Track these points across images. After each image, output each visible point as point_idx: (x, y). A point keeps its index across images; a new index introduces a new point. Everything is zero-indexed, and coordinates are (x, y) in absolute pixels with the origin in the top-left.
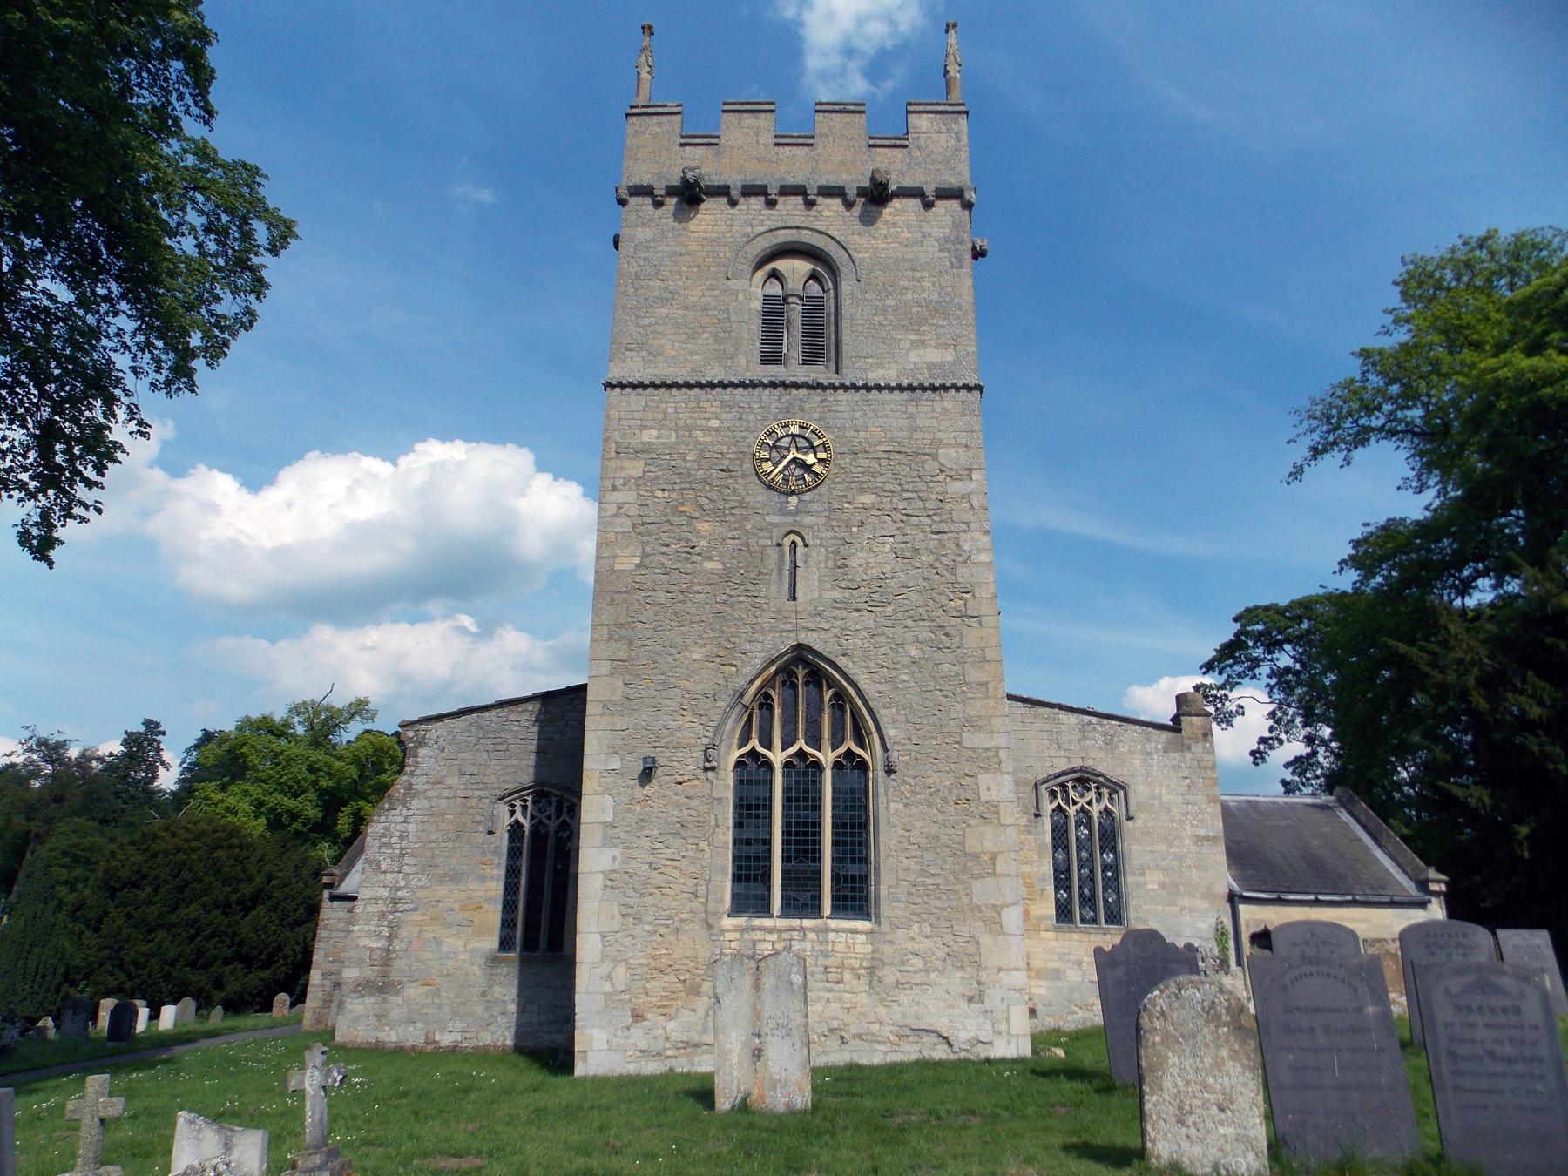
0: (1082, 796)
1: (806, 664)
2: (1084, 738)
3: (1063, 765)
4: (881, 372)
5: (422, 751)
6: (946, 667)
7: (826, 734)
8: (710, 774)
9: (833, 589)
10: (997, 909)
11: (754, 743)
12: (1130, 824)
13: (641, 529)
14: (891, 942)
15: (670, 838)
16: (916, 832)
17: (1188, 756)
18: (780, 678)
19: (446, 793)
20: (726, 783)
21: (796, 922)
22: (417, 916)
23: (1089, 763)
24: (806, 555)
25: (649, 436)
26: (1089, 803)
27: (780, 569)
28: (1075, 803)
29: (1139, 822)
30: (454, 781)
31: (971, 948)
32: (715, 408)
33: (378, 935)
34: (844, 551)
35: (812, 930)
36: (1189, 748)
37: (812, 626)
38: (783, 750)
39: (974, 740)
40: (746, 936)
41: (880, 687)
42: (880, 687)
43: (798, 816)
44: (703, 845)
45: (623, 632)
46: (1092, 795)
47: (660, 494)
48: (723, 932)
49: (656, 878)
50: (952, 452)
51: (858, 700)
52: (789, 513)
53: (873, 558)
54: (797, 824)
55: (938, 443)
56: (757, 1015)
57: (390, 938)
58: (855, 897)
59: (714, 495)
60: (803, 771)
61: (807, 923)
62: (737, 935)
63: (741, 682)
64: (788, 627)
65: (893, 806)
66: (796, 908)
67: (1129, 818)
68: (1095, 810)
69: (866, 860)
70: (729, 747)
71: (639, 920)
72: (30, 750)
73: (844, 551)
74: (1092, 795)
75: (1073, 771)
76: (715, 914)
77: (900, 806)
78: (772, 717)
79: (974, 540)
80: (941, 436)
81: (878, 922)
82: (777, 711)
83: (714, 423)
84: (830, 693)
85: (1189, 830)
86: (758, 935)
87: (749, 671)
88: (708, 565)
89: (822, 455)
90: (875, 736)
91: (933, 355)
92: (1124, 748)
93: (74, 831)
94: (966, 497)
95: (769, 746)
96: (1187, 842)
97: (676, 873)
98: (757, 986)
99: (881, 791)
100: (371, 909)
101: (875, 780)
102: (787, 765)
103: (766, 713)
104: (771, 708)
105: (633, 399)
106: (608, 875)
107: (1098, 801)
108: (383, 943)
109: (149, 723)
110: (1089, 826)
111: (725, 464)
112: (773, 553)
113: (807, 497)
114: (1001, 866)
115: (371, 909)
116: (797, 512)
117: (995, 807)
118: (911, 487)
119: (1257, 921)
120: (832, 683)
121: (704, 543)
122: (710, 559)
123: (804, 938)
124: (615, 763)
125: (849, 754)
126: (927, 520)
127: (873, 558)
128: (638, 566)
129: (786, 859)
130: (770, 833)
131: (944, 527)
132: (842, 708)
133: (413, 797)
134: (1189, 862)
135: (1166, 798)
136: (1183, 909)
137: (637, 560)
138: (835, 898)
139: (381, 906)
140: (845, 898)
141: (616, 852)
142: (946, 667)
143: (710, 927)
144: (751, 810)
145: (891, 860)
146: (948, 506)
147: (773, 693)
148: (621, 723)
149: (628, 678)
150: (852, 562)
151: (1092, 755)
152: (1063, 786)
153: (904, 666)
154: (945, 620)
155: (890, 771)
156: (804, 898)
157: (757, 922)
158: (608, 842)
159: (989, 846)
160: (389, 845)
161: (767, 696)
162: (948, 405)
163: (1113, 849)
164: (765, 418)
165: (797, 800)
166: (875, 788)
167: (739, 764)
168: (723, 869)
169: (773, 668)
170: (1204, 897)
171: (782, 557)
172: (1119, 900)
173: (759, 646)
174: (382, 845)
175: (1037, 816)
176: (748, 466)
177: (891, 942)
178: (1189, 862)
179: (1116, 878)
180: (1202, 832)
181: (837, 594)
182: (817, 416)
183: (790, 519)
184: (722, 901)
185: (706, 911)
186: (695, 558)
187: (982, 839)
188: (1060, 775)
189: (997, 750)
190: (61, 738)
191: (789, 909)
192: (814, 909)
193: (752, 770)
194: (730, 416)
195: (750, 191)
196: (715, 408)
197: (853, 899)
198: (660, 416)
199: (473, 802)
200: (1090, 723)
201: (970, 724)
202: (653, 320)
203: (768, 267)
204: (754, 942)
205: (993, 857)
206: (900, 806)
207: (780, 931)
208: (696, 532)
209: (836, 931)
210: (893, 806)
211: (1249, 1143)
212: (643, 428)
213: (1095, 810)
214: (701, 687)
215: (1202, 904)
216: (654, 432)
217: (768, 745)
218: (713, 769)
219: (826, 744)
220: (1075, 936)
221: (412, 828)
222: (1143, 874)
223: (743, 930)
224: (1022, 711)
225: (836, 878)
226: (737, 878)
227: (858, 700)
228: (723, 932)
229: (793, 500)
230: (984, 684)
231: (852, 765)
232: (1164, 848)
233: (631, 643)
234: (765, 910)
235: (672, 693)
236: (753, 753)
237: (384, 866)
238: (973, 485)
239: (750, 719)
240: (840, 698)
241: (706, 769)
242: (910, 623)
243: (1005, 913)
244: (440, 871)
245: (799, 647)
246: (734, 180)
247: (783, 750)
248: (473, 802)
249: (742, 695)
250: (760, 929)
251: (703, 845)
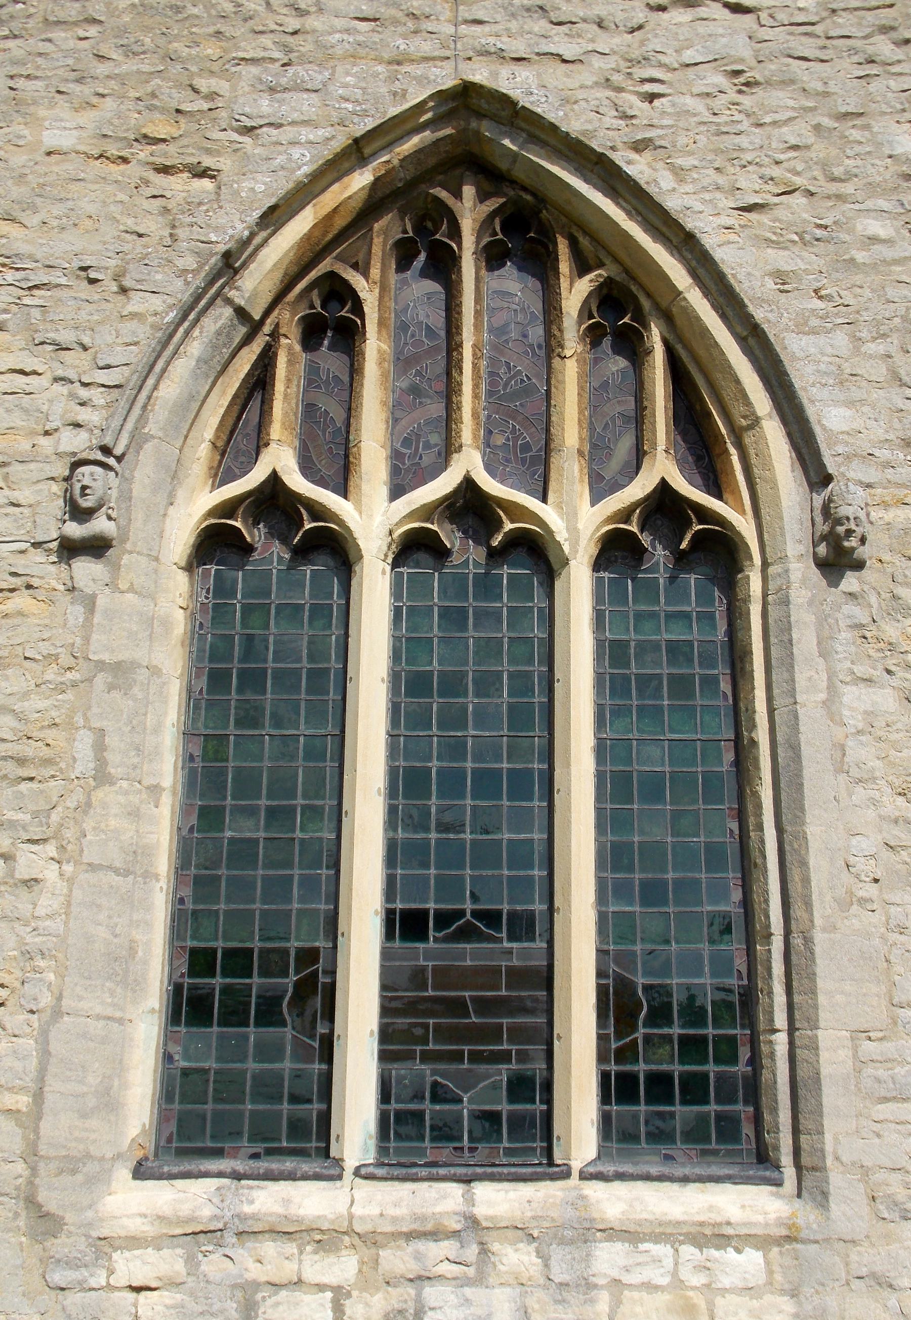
1: (491, 175)
7: (570, 432)
8: (85, 569)
11: (281, 459)
14: (882, 1283)
18: (386, 230)
20: (155, 603)
21: (442, 1199)
35: (521, 1231)
37: (518, 47)
38: (397, 492)
40: (213, 1265)
41: (781, 259)
42: (781, 259)
43: (456, 750)
48: (104, 1246)
51: (697, 301)
54: (452, 783)
58: (703, 1078)
61: (496, 1199)
62: (166, 1262)
63: (231, 225)
64: (427, 47)
65: (854, 698)
66: (445, 1132)
70: (174, 474)
76: (71, 1165)
77: (885, 699)
78: (355, 370)
81: (810, 1177)
84: (584, 286)
86: (271, 1260)
87: (263, 188)
90: (773, 436)
99: (805, 639)
101: (777, 600)
103: (330, 361)
104: (348, 336)
120: (595, 247)
123: (482, 1271)
125: (664, 506)
130: (332, 925)
132: (631, 345)
138: (616, 1088)
140: (660, 1087)
143: (44, 1222)
145: (859, 919)
147: (358, 282)
153: (872, 189)
155: (837, 558)
156: (485, 1089)
157: (268, 1199)
161: (338, 292)
165: (452, 684)
166: (779, 632)
167: (217, 544)
168: (121, 965)
169: (361, 180)
173: (305, 105)
177: (882, 1283)
184: (109, 1103)
185: (32, 1154)
191: (415, 1135)
192: (521, 1135)
193: (268, 544)
197: (694, 1090)
206: (885, 699)
207: (372, 1240)
209: (629, 1235)
210: (854, 698)
214: (68, 246)
218: (97, 547)
219: (570, 469)
223: (202, 1236)
226: (188, 1007)
227: (697, 301)
228: (104, 1246)
231: (681, 548)
236: (273, 501)
239: (260, 382)
241: (70, 549)
243: (480, 1211)
245: (465, 100)
247: (397, 492)
249: (230, 264)
250: (284, 1231)
251: (30, 861)
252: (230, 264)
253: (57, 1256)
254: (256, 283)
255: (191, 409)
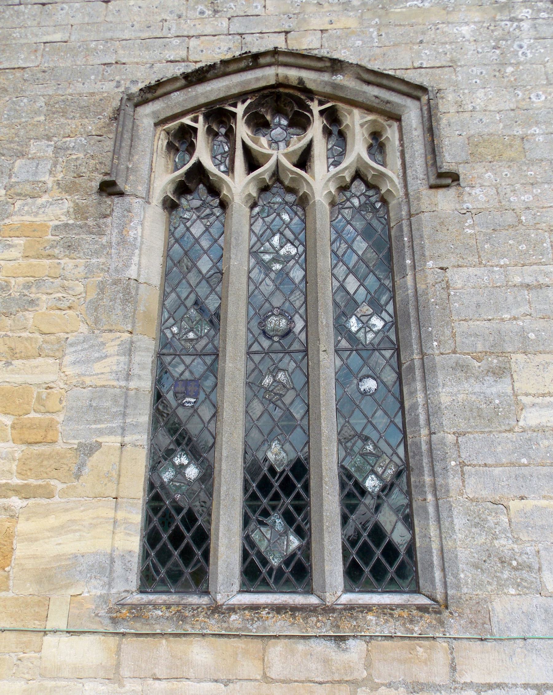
12: (445, 201)
26: (304, 160)
29: (479, 191)
61: (194, 599)
67: (445, 179)
107: (335, 159)
175: (108, 188)
211: (259, 675)
220: (200, 653)
222: (501, 372)
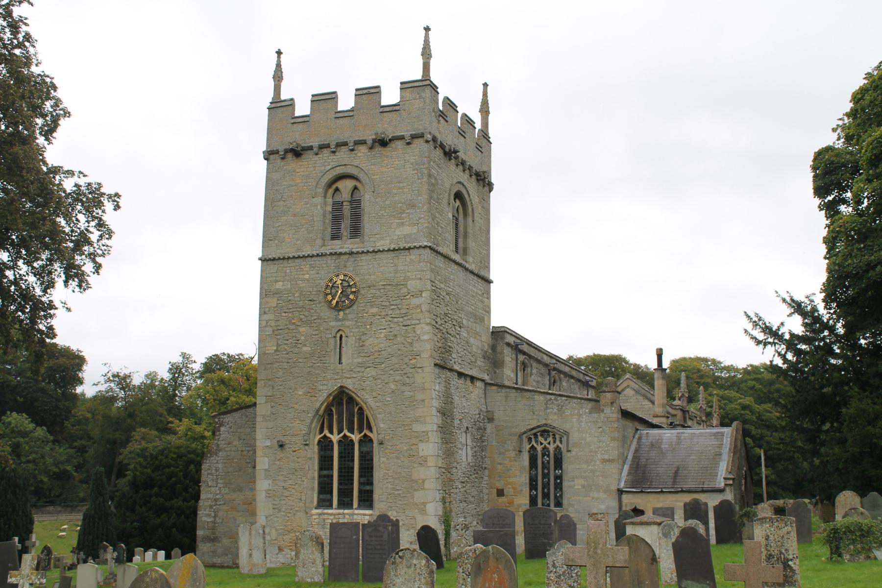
0: (546, 440)
2: (547, 408)
3: (534, 424)
4: (382, 242)
5: (222, 429)
6: (407, 393)
9: (358, 357)
10: (424, 504)
12: (569, 454)
13: (276, 332)
15: (291, 476)
16: (391, 471)
17: (602, 415)
19: (233, 449)
21: (341, 511)
22: (225, 507)
23: (549, 422)
24: (346, 341)
25: (279, 285)
26: (549, 443)
27: (335, 349)
28: (542, 444)
29: (573, 453)
30: (236, 443)
31: (412, 522)
32: (307, 268)
33: (209, 515)
34: (363, 338)
36: (603, 411)
39: (417, 427)
41: (378, 404)
42: (378, 404)
44: (304, 479)
45: (270, 383)
46: (550, 439)
47: (284, 314)
48: (312, 515)
49: (287, 493)
50: (413, 282)
52: (340, 320)
53: (376, 341)
55: (407, 279)
56: (250, 543)
57: (215, 517)
59: (306, 313)
60: (347, 445)
61: (346, 511)
65: (382, 459)
66: (344, 505)
67: (569, 451)
68: (551, 448)
69: (372, 484)
71: (280, 511)
72: (109, 380)
73: (363, 338)
74: (550, 439)
75: (539, 427)
79: (422, 328)
80: (409, 274)
82: (335, 417)
83: (307, 276)
85: (599, 456)
86: (326, 517)
87: (321, 399)
88: (305, 349)
89: (353, 290)
91: (407, 230)
92: (568, 413)
93: (143, 438)
94: (419, 306)
95: (332, 433)
96: (598, 463)
97: (294, 491)
98: (250, 534)
100: (206, 504)
102: (340, 442)
105: (272, 266)
106: (267, 491)
107: (554, 442)
108: (212, 519)
109: (184, 355)
110: (548, 456)
111: (311, 297)
112: (332, 341)
113: (347, 311)
114: (427, 485)
115: (206, 504)
116: (343, 320)
117: (425, 459)
118: (394, 303)
119: (631, 504)
121: (303, 338)
122: (305, 345)
124: (268, 443)
126: (401, 320)
127: (376, 341)
128: (276, 351)
129: (340, 484)
131: (409, 322)
133: (220, 451)
134: (598, 473)
135: (588, 439)
136: (593, 498)
137: (275, 348)
139: (210, 503)
141: (270, 481)
142: (407, 393)
143: (307, 513)
144: (325, 462)
146: (411, 312)
148: (270, 425)
149: (273, 404)
150: (367, 343)
151: (550, 417)
152: (535, 435)
154: (408, 370)
156: (346, 500)
157: (326, 511)
158: (267, 477)
159: (422, 477)
160: (211, 474)
162: (413, 257)
163: (561, 468)
164: (329, 272)
167: (319, 441)
170: (604, 492)
171: (336, 343)
172: (561, 495)
173: (325, 387)
174: (208, 474)
176: (321, 298)
178: (598, 473)
179: (561, 483)
180: (606, 457)
181: (360, 360)
182: (352, 269)
183: (340, 323)
184: (312, 502)
186: (299, 346)
187: (420, 473)
188: (533, 429)
189: (428, 432)
190: (127, 373)
193: (325, 445)
194: (313, 272)
195: (322, 147)
196: (307, 268)
198: (283, 275)
199: (245, 453)
200: (551, 399)
201: (417, 420)
202: (280, 224)
203: (334, 187)
204: (324, 520)
205: (424, 481)
206: (385, 459)
208: (299, 332)
210: (382, 459)
212: (276, 281)
213: (551, 448)
215: (602, 496)
216: (281, 283)
217: (331, 432)
221: (220, 466)
223: (320, 514)
224: (515, 394)
225: (360, 491)
229: (341, 313)
230: (423, 401)
231: (366, 441)
232: (585, 466)
233: (273, 388)
234: (330, 506)
235: (290, 411)
237: (210, 484)
238: (423, 299)
240: (361, 409)
242: (392, 372)
244: (233, 486)
246: (315, 143)
247: (339, 434)
248: (245, 453)
251: (304, 479)
252: (318, 411)
253: (428, 275)
254: (321, 412)
255: (316, 427)
